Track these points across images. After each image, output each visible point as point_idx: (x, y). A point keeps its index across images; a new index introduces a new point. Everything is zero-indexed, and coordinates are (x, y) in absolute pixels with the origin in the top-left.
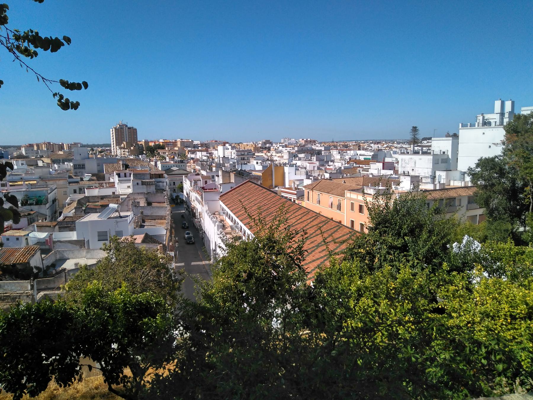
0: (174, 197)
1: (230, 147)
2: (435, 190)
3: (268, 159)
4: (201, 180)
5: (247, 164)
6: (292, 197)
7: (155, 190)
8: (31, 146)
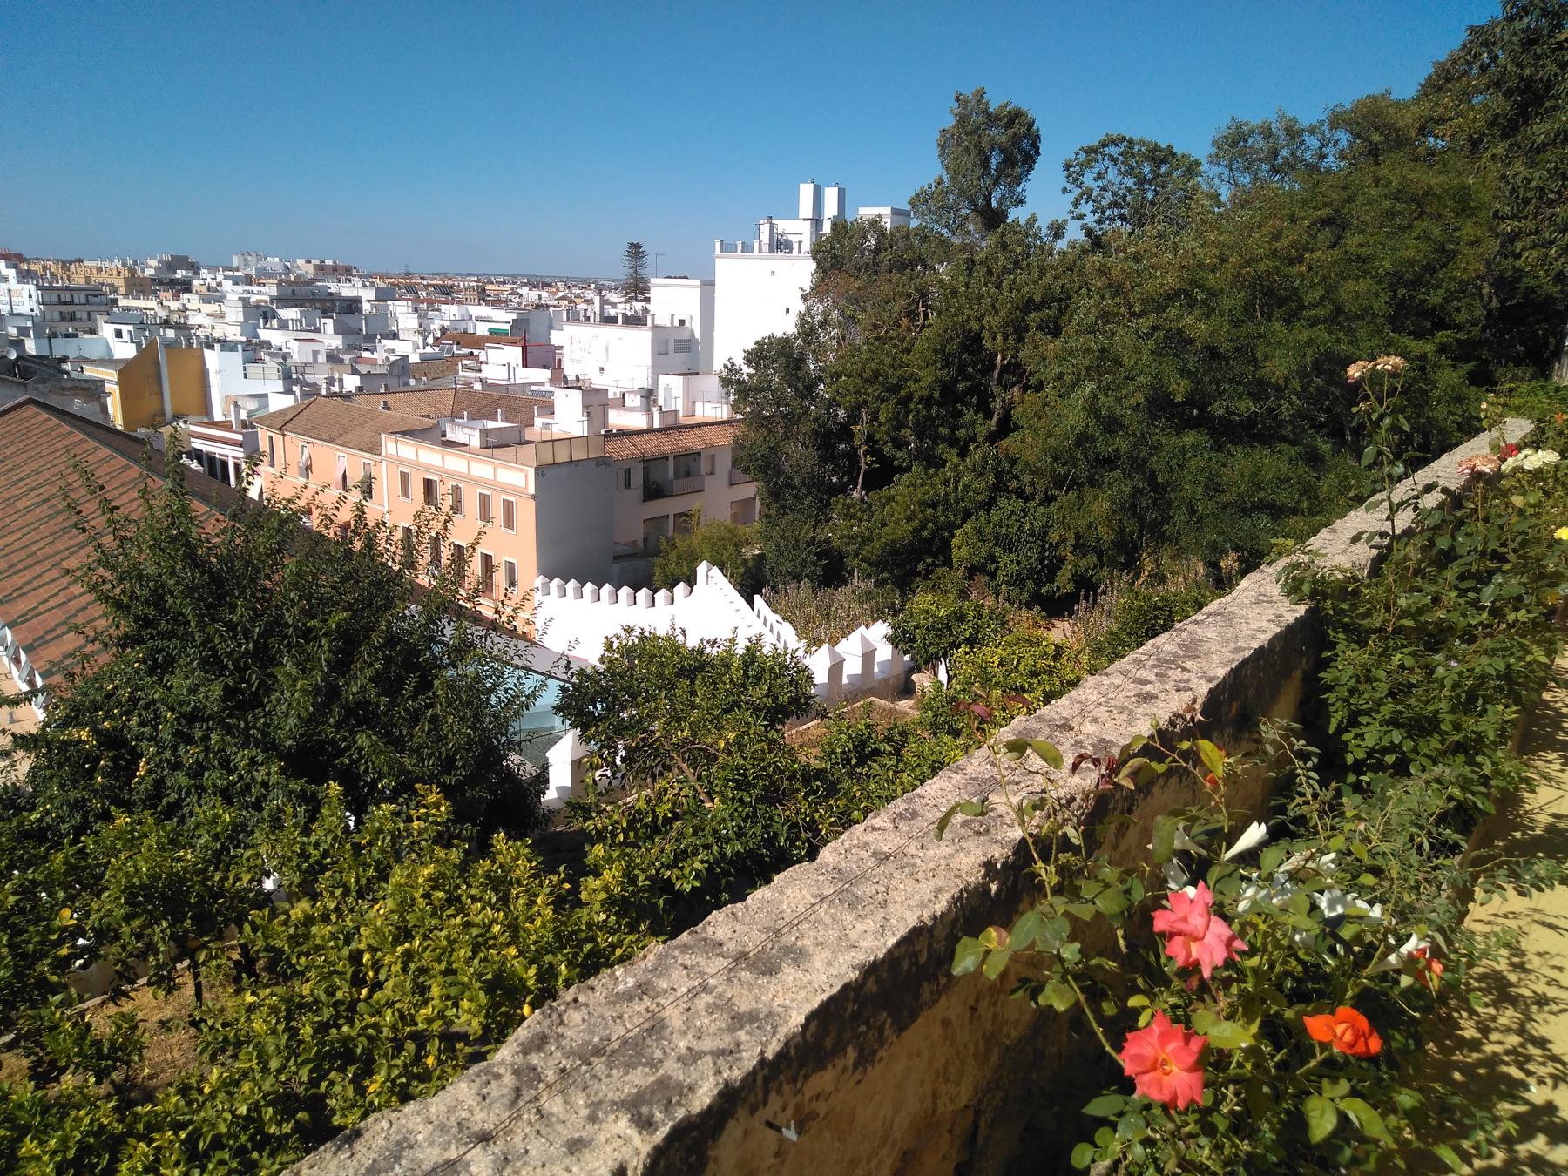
2: (651, 431)
5: (75, 336)
6: (230, 453)
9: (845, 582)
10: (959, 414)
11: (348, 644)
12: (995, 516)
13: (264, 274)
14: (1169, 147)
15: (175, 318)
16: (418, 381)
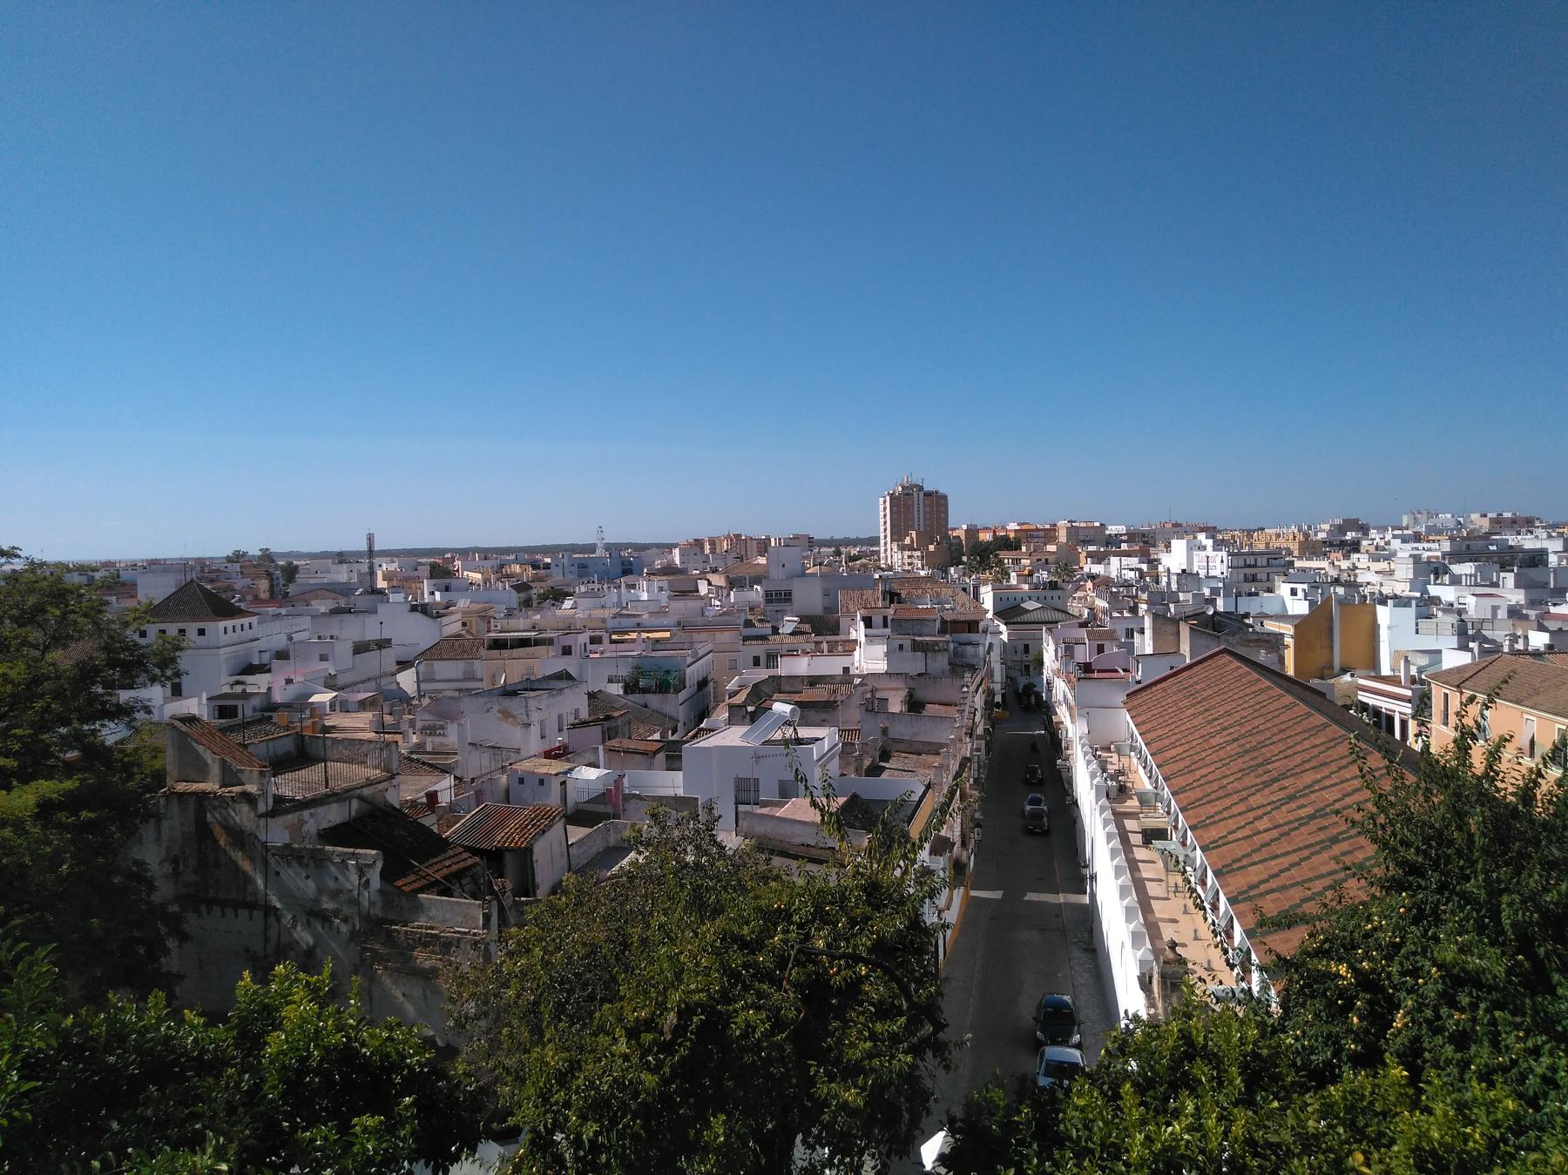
0: (1021, 687)
1: (1209, 543)
3: (1337, 581)
4: (1087, 641)
5: (1256, 594)
7: (947, 667)
8: (699, 543)
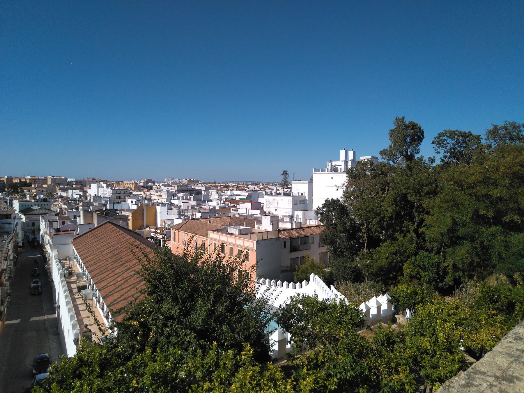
1: (105, 185)
2: (292, 229)
4: (58, 220)
5: (120, 203)
9: (362, 281)
10: (403, 222)
11: (219, 295)
12: (418, 258)
13: (173, 183)
14: (470, 132)
15: (148, 197)
16: (219, 214)
